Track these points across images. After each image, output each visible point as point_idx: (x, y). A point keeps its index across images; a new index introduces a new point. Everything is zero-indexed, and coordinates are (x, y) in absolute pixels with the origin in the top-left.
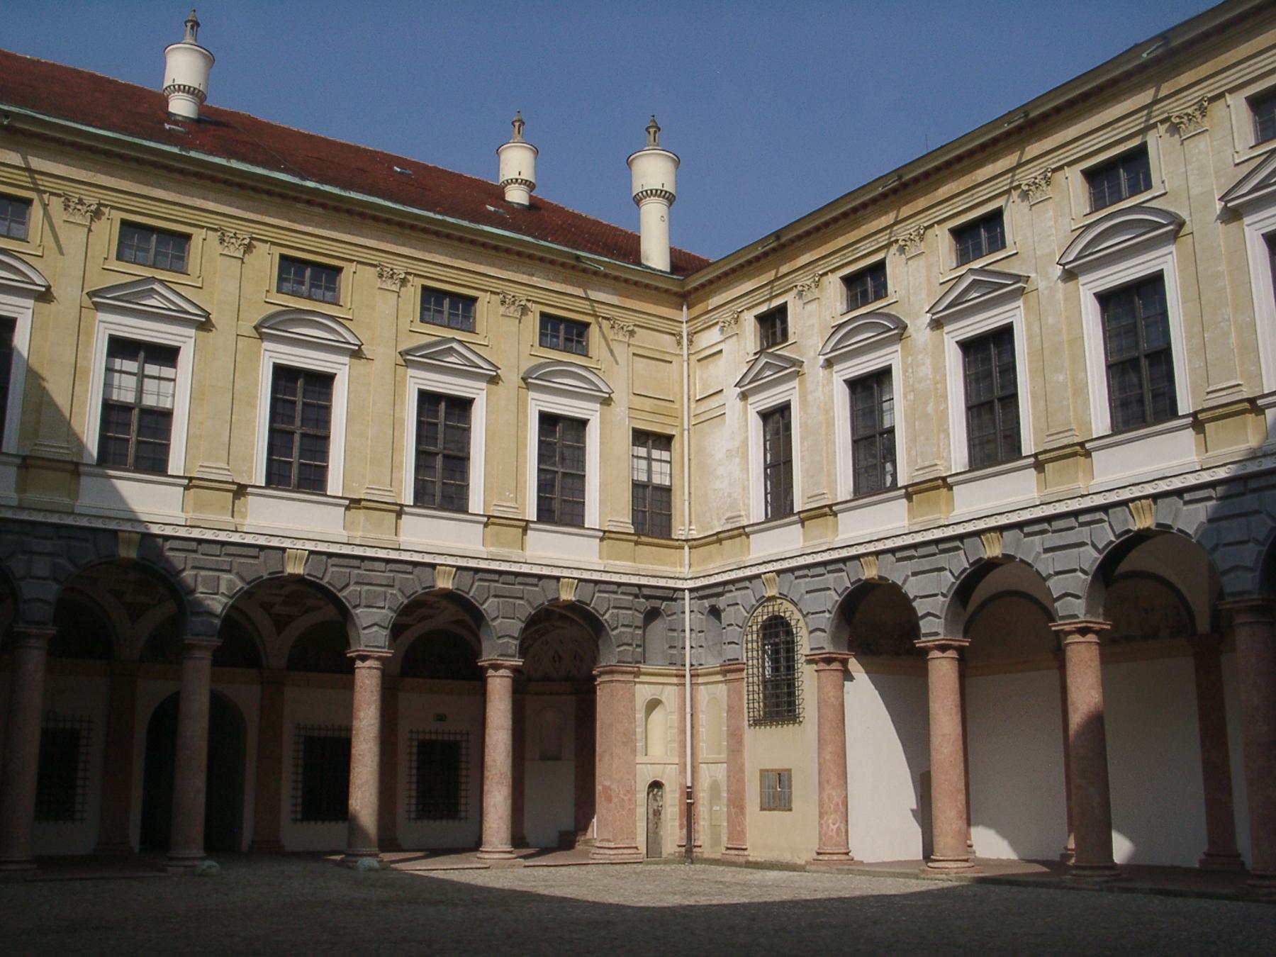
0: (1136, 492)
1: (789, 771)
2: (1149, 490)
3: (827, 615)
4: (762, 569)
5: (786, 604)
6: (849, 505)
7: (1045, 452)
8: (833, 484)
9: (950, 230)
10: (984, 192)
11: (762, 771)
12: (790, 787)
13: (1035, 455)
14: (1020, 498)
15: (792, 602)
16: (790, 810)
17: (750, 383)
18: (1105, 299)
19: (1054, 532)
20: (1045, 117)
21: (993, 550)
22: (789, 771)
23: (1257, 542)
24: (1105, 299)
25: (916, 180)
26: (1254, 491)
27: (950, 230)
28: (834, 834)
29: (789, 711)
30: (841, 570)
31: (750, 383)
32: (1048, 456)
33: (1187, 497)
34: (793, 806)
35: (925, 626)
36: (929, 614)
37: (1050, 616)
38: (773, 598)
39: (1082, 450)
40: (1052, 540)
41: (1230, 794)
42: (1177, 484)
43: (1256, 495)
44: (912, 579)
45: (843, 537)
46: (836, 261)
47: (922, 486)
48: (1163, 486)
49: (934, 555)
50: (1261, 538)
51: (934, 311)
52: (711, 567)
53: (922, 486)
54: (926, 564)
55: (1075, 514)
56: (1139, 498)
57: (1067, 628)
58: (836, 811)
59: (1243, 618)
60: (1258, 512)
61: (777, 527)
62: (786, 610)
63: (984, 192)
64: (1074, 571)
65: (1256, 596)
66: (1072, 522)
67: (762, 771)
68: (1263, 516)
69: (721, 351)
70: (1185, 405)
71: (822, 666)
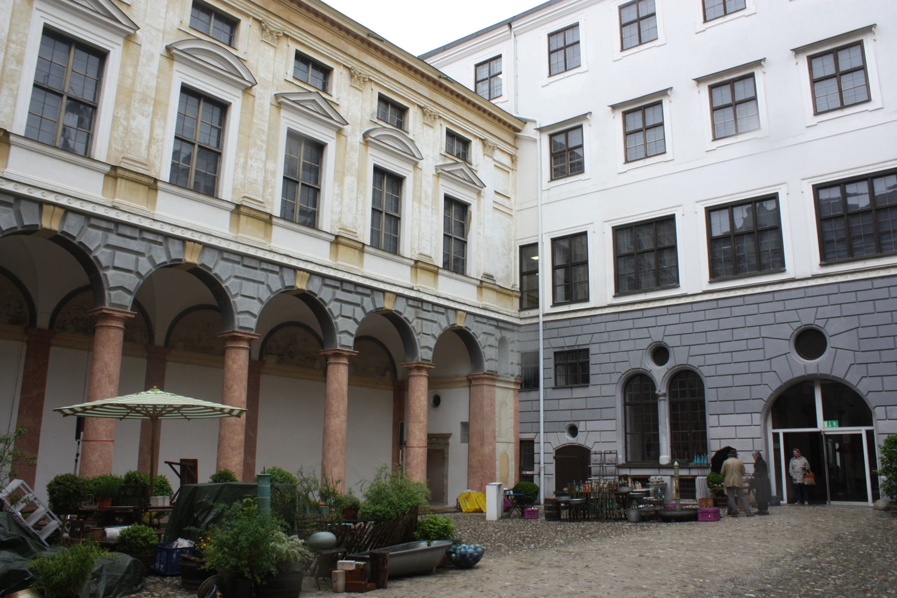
0: (196, 237)
2: (204, 239)
14: (318, 257)
17: (293, 101)
19: (244, 266)
23: (260, 300)
26: (263, 269)
31: (293, 101)
32: (127, 174)
33: (226, 255)
36: (346, 332)
40: (114, 240)
43: (264, 273)
45: (367, 271)
47: (505, 291)
49: (255, 268)
50: (143, 273)
53: (505, 291)
55: (142, 229)
56: (195, 241)
57: (117, 314)
60: (262, 283)
61: (452, 278)
64: (254, 298)
65: (129, 310)
66: (136, 234)
68: (265, 286)
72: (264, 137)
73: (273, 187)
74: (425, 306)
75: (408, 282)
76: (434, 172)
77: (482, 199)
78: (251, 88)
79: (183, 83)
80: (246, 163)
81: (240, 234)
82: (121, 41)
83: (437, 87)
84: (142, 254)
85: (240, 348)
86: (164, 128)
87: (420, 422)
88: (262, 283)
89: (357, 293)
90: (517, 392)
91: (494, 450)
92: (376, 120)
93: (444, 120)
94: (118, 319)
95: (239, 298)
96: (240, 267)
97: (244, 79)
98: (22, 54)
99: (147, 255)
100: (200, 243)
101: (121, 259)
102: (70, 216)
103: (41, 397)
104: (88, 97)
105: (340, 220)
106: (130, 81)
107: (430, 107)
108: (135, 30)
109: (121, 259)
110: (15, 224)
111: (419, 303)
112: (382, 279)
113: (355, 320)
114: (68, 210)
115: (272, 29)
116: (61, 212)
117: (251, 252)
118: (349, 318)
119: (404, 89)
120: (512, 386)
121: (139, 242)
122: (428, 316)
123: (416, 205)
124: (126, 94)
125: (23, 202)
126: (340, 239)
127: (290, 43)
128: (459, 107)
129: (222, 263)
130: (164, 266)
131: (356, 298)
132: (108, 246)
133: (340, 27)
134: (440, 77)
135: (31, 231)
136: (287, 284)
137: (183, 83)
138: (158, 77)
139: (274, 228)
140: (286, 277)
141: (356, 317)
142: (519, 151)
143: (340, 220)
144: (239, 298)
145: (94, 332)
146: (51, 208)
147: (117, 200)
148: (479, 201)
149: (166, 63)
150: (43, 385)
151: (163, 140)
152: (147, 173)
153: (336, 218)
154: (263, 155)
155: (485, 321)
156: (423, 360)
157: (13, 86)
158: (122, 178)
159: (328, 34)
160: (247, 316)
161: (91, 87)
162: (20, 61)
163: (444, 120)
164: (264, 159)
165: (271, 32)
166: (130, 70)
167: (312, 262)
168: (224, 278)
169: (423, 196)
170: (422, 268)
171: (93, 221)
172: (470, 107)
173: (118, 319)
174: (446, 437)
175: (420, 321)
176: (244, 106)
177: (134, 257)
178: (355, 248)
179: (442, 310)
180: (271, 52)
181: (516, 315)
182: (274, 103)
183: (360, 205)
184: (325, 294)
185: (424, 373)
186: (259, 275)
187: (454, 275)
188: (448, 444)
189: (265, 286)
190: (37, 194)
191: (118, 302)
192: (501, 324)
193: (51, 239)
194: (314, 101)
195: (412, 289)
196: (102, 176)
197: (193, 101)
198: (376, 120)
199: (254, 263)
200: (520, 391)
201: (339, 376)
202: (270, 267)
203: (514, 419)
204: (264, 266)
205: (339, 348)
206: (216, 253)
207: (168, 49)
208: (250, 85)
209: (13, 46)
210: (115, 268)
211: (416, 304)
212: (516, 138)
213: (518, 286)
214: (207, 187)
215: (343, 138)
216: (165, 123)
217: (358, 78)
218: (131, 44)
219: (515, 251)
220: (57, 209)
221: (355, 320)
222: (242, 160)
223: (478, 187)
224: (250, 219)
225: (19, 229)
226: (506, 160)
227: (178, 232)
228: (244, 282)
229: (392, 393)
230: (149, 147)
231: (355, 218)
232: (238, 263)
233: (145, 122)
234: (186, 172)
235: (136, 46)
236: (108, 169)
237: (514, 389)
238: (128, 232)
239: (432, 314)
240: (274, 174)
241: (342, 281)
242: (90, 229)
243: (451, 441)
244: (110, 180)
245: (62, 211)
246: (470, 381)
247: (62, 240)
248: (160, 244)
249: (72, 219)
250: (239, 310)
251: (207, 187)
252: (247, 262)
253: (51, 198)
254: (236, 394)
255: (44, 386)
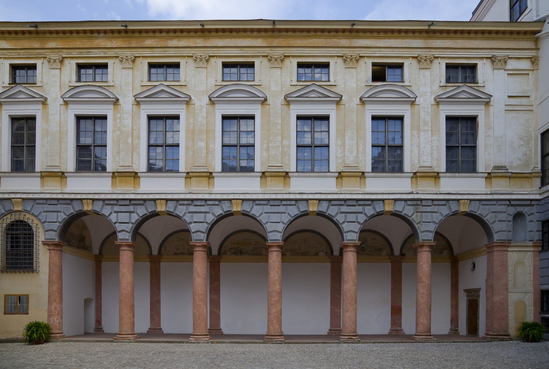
0: (237, 197)
1: (27, 296)
2: (242, 197)
3: (58, 224)
4: (12, 196)
5: (28, 216)
6: (7, 174)
7: (193, 172)
8: (289, 165)
9: (77, 63)
10: (171, 52)
11: (5, 296)
12: (28, 303)
13: (41, 172)
15: (33, 214)
16: (28, 314)
18: (449, 119)
20: (210, 31)
21: (87, 207)
22: (27, 296)
23: (283, 223)
24: (449, 119)
25: (133, 31)
26: (284, 205)
27: (77, 63)
28: (57, 324)
29: (30, 267)
30: (69, 204)
31: (69, 97)
32: (194, 174)
33: (257, 202)
34: (30, 312)
35: (120, 236)
36: (123, 230)
37: (265, 240)
38: (19, 211)
39: (62, 175)
41: (219, 309)
42: (254, 197)
43: (285, 207)
44: (264, 215)
45: (368, 189)
46: (75, 53)
48: (248, 197)
49: (355, 206)
50: (209, 222)
51: (138, 96)
52: (516, 190)
54: (123, 209)
57: (198, 244)
58: (58, 314)
59: (126, 248)
60: (285, 213)
62: (28, 218)
63: (250, 52)
64: (279, 222)
65: (130, 241)
66: (203, 203)
67: (5, 296)
68: (287, 214)
69: (528, 74)
70: (38, 168)
71: (52, 248)
72: (279, 127)
73: (289, 155)
74: (424, 203)
75: (409, 189)
76: (433, 102)
77: (491, 108)
78: (489, 101)
79: (75, 115)
80: (268, 146)
81: (343, 189)
82: (184, 106)
83: (431, 34)
84: (208, 213)
85: (272, 251)
86: (214, 144)
87: (423, 282)
88: (285, 213)
89: (359, 205)
90: (537, 253)
91: (506, 299)
92: (371, 84)
93: (217, 56)
94: (199, 246)
95: (269, 224)
96: (269, 207)
97: (259, 97)
98: (139, 134)
99: (211, 212)
100: (468, 199)
101: (196, 217)
102: (169, 202)
103: (219, 286)
104: (398, 142)
105: (344, 161)
106: (192, 125)
107: (348, 52)
108: (490, 98)
109: (196, 217)
110: (145, 212)
111: (417, 202)
112: (382, 192)
113: (358, 222)
114: (167, 200)
115: (276, 57)
116: (91, 201)
117: (121, 197)
118: (354, 222)
119: (462, 51)
120: (532, 249)
121: (206, 207)
122: (429, 209)
123: (415, 133)
124: (191, 133)
125: (147, 202)
126: (342, 174)
127: (366, 60)
128: (460, 41)
129: (481, 207)
130: (448, 216)
131: (360, 209)
132: (189, 212)
133: (302, 31)
134: (36, 27)
135: (305, 214)
136: (301, 210)
137: (75, 115)
138: (207, 117)
139: (442, 179)
140: (300, 206)
141: (359, 221)
142: (540, 51)
143: (344, 161)
144: (269, 224)
145: (193, 254)
146: (160, 201)
147: (493, 189)
148: (487, 110)
149: (210, 107)
150: (219, 280)
151: (214, 150)
152: (358, 171)
153: (340, 161)
154: (279, 138)
155: (495, 202)
156: (423, 240)
157: (138, 151)
158: (293, 177)
159: (321, 40)
160: (275, 233)
161: (398, 136)
162: (139, 138)
163: (217, 56)
164: (280, 140)
165: (276, 59)
166: (191, 120)
167: (13, 193)
168: (257, 215)
169: (422, 124)
170: (421, 177)
171: (180, 202)
172: (473, 35)
173: (199, 246)
174: (478, 290)
175: (420, 214)
176: (412, 115)
177: (203, 215)
178: (356, 176)
179: (444, 203)
180: (278, 71)
181: (539, 192)
182: (284, 103)
183: (361, 147)
184: (332, 211)
185: (426, 249)
186: (282, 209)
187: (457, 174)
188: (479, 296)
189: (287, 214)
190: (79, 197)
191: (198, 238)
192: (512, 203)
193: (464, 215)
194: (313, 90)
195: (412, 193)
196: (484, 179)
197: (381, 123)
198: (371, 84)
199: (277, 203)
200: (540, 252)
201: (275, 257)
202: (288, 203)
203: (534, 274)
204: (284, 203)
205: (345, 242)
206: (251, 202)
207: (361, 99)
208: (339, 99)
209: (135, 132)
210: (195, 222)
211: (415, 203)
212: (537, 40)
213: (540, 168)
214: (397, 167)
215: (342, 106)
216: (215, 141)
217: (351, 60)
218: (190, 106)
219: (536, 140)
220: (162, 201)
221: (358, 222)
222: (265, 146)
223: (487, 101)
224: (273, 178)
225: (451, 214)
226: (525, 65)
227: (225, 197)
228: (271, 214)
229: (450, 264)
230: (207, 157)
231: (357, 157)
232: (267, 205)
233: (203, 144)
234: (21, 162)
235: (192, 106)
236: (486, 175)
237: (533, 251)
238: (199, 203)
239: (433, 207)
240: (289, 146)
241: (345, 200)
242: (179, 207)
243: (481, 293)
244: (488, 179)
245: (91, 201)
246: (490, 247)
247: (320, 214)
248: (218, 205)
249: (325, 204)
250: (346, 231)
251: (397, 167)
252: (272, 203)
253: (84, 196)
254: (272, 276)
255: (219, 281)
